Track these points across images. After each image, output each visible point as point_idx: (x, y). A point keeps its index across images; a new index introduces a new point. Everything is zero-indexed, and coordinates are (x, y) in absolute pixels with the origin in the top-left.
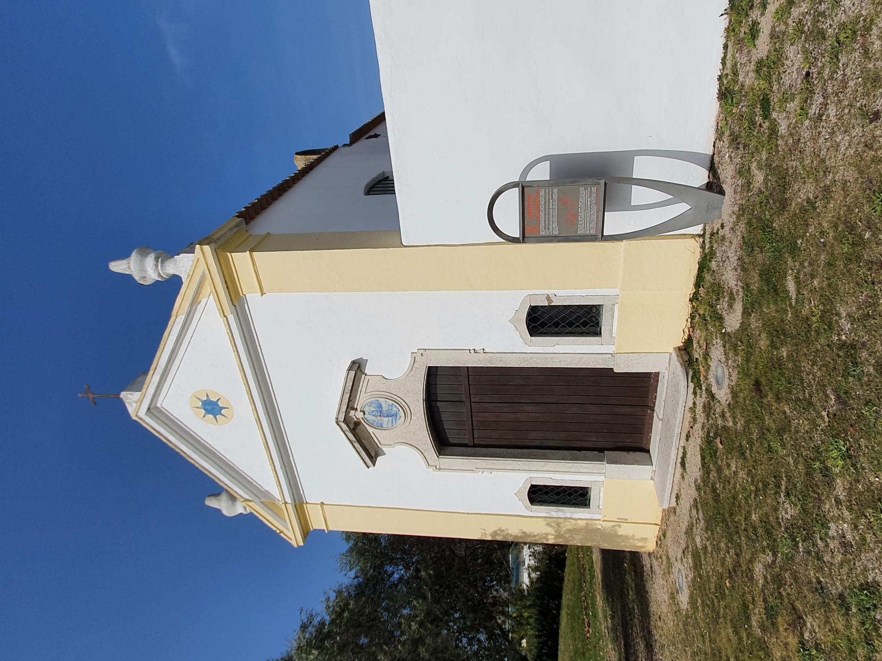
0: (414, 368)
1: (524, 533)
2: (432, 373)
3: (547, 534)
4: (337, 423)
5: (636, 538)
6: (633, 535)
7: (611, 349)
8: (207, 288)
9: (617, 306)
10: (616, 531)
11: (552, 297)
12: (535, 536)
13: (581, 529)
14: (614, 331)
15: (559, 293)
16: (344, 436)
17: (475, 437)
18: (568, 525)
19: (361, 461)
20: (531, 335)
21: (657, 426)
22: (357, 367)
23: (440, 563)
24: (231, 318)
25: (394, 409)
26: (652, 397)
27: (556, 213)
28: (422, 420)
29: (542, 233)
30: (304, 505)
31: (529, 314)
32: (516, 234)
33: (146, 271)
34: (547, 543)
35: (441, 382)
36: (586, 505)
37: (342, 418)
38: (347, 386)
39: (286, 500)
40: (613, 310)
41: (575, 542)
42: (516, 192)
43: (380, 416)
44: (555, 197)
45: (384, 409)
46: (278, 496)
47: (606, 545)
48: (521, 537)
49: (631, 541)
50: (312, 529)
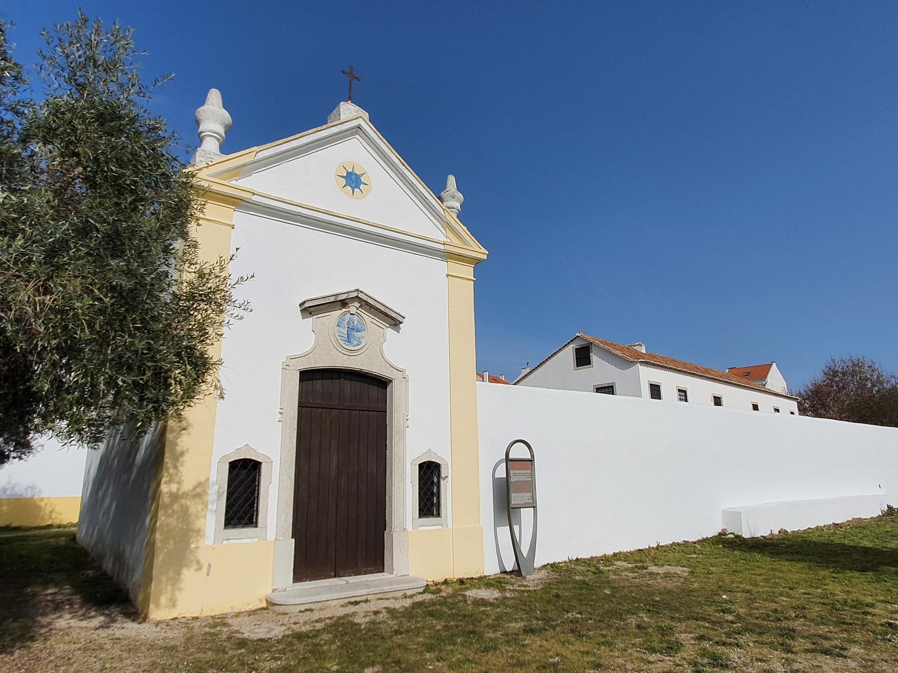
0: (392, 369)
1: (182, 454)
2: (382, 383)
3: (179, 483)
4: (357, 290)
5: (177, 593)
6: (181, 589)
7: (409, 527)
8: (456, 241)
9: (440, 527)
10: (188, 566)
11: (446, 480)
12: (175, 467)
13: (188, 524)
14: (423, 528)
15: (449, 485)
16: (344, 291)
17: (370, 412)
18: (194, 507)
19: (315, 297)
20: (230, 463)
21: (353, 579)
22: (395, 323)
23: (114, 338)
24: (442, 247)
25: (355, 342)
26: (349, 573)
27: (521, 480)
28: (343, 364)
29: (511, 472)
30: (234, 208)
31: (250, 460)
32: (511, 457)
33: (456, 201)
34: (162, 482)
35: (374, 390)
36: (252, 523)
37: (361, 295)
38: (392, 312)
39: (255, 196)
40: (438, 525)
41: (163, 518)
42: (529, 457)
43: (348, 327)
44: (527, 479)
45: (355, 333)
46: (233, 183)
47: (160, 558)
48: (173, 450)
49: (169, 588)
50: (485, 257)
